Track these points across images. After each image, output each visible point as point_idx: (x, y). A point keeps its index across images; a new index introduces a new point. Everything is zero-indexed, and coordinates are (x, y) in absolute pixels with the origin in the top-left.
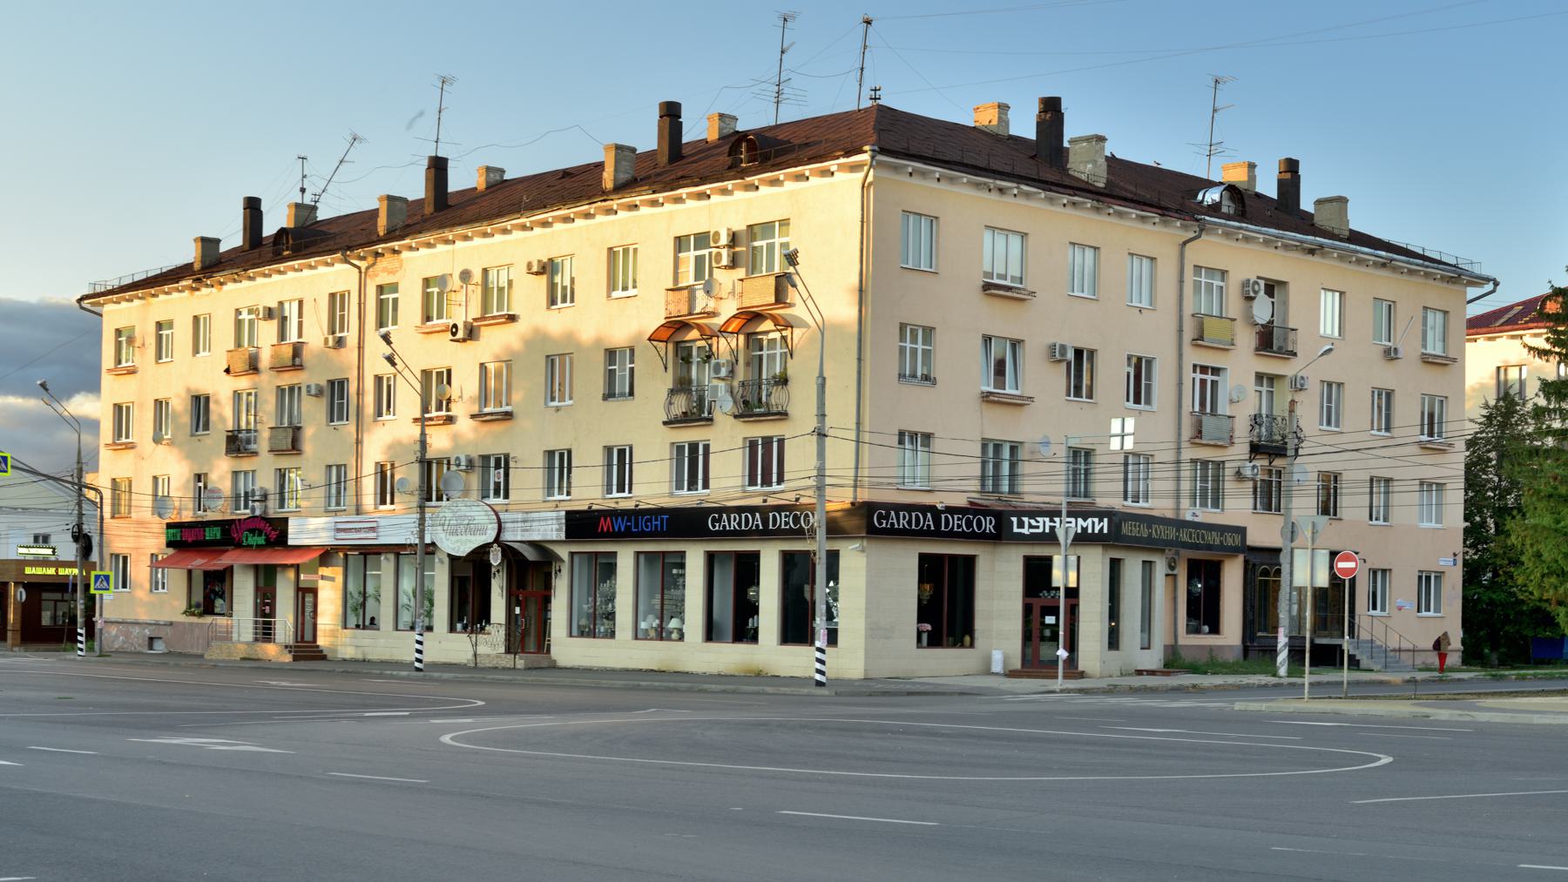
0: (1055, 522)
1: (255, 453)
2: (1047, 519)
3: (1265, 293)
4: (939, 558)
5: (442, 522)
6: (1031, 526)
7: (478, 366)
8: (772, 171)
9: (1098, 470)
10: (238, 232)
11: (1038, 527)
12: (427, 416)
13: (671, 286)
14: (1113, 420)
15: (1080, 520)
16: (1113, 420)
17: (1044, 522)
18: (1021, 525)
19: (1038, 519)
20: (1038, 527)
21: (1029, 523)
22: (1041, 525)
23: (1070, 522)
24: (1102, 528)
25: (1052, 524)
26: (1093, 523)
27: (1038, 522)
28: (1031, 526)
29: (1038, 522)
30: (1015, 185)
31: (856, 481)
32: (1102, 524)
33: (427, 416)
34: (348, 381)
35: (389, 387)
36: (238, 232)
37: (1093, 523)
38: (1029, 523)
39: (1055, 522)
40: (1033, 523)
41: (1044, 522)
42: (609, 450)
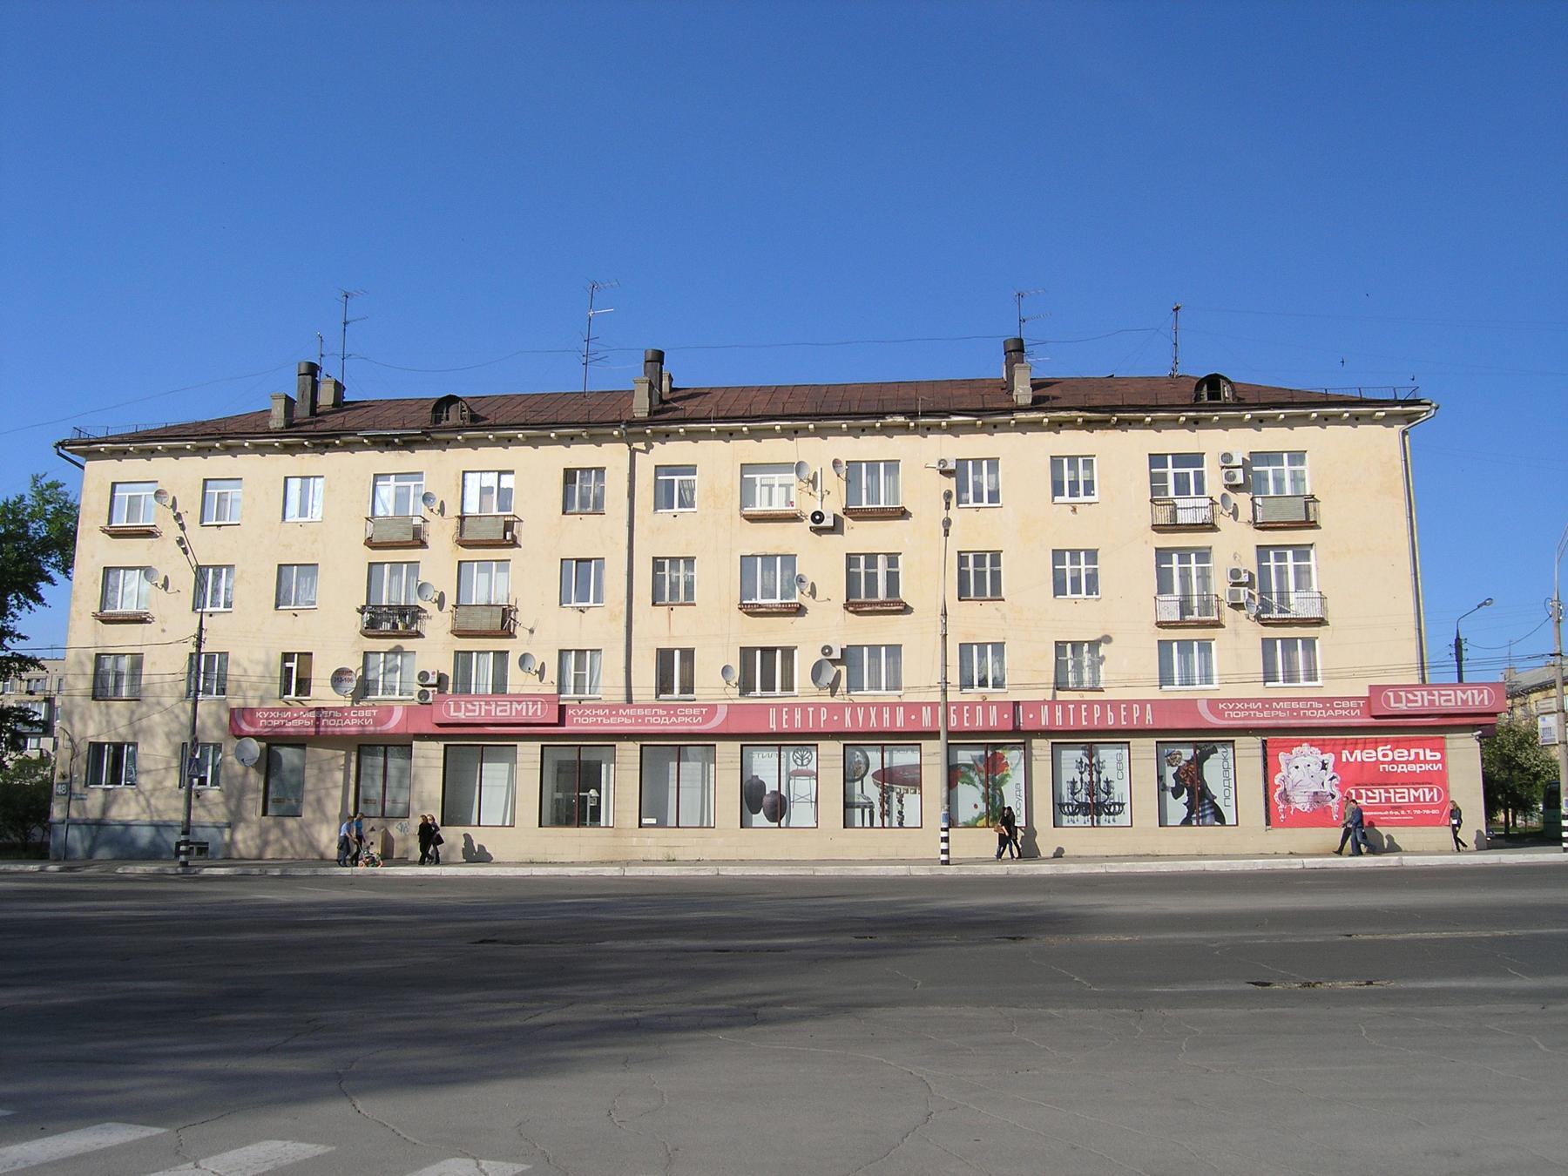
0: (1434, 695)
1: (1278, 681)
2: (1425, 693)
3: (448, 677)
7: (651, 559)
8: (885, 901)
13: (455, 603)
14: (671, 763)
15: (1412, 791)
16: (671, 763)
19: (1416, 693)
22: (1419, 698)
24: (1483, 699)
25: (1387, 795)
26: (1424, 792)
27: (1374, 793)
29: (1374, 793)
34: (851, 554)
38: (1407, 697)
39: (1434, 695)
40: (1370, 794)
42: (997, 594)
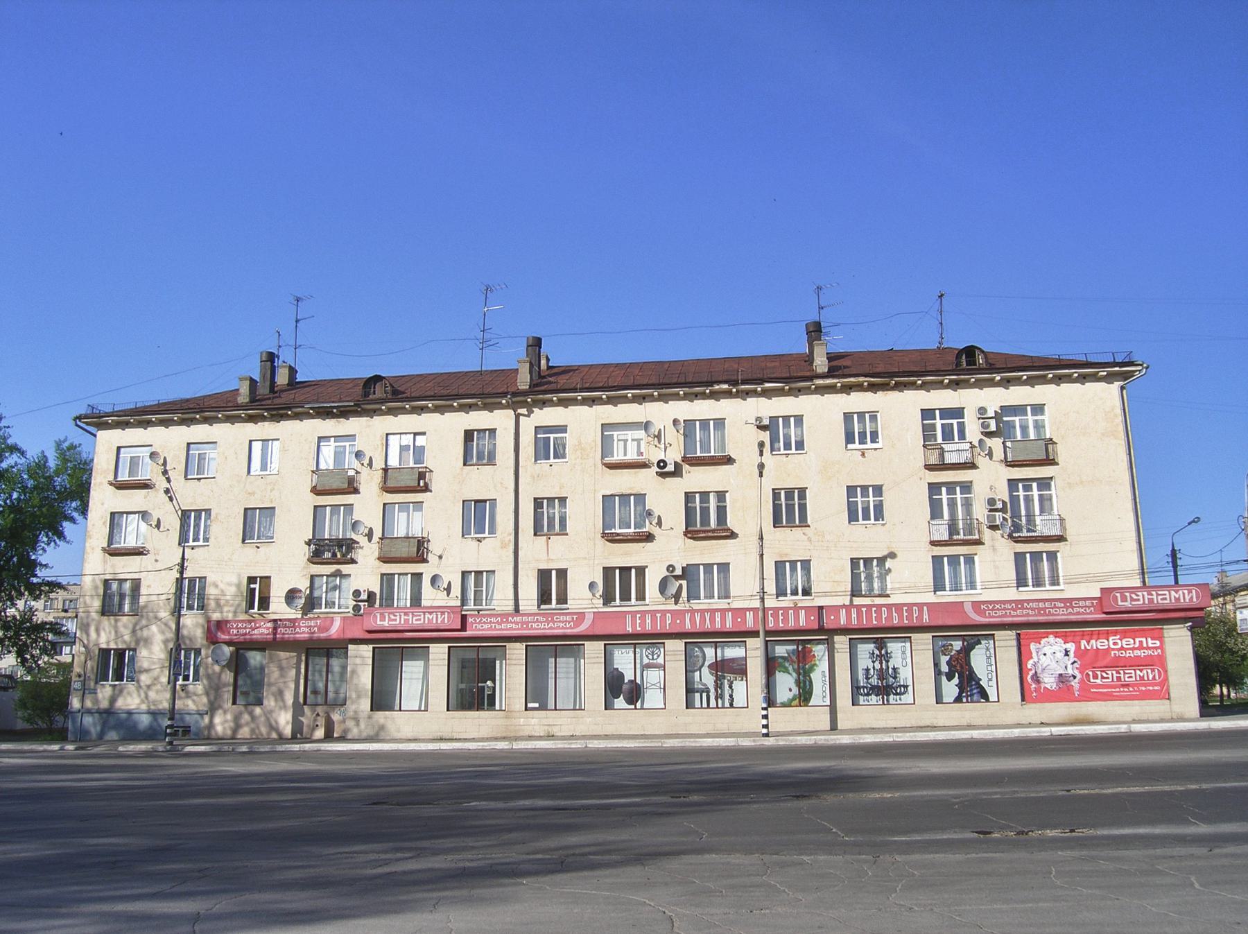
4: (708, 453)
5: (1064, 681)
6: (1132, 599)
9: (514, 657)
10: (925, 473)
11: (1138, 600)
12: (955, 537)
17: (1112, 674)
18: (1124, 599)
20: (1138, 600)
21: (1102, 675)
22: (1141, 598)
23: (1152, 644)
27: (1138, 596)
28: (1103, 677)
29: (1138, 596)
30: (838, 381)
31: (961, 450)
32: (1191, 594)
33: (955, 537)
35: (723, 810)
36: (925, 473)
37: (1184, 594)
38: (1102, 675)
39: (1152, 595)
40: (1105, 675)
41: (1112, 674)
